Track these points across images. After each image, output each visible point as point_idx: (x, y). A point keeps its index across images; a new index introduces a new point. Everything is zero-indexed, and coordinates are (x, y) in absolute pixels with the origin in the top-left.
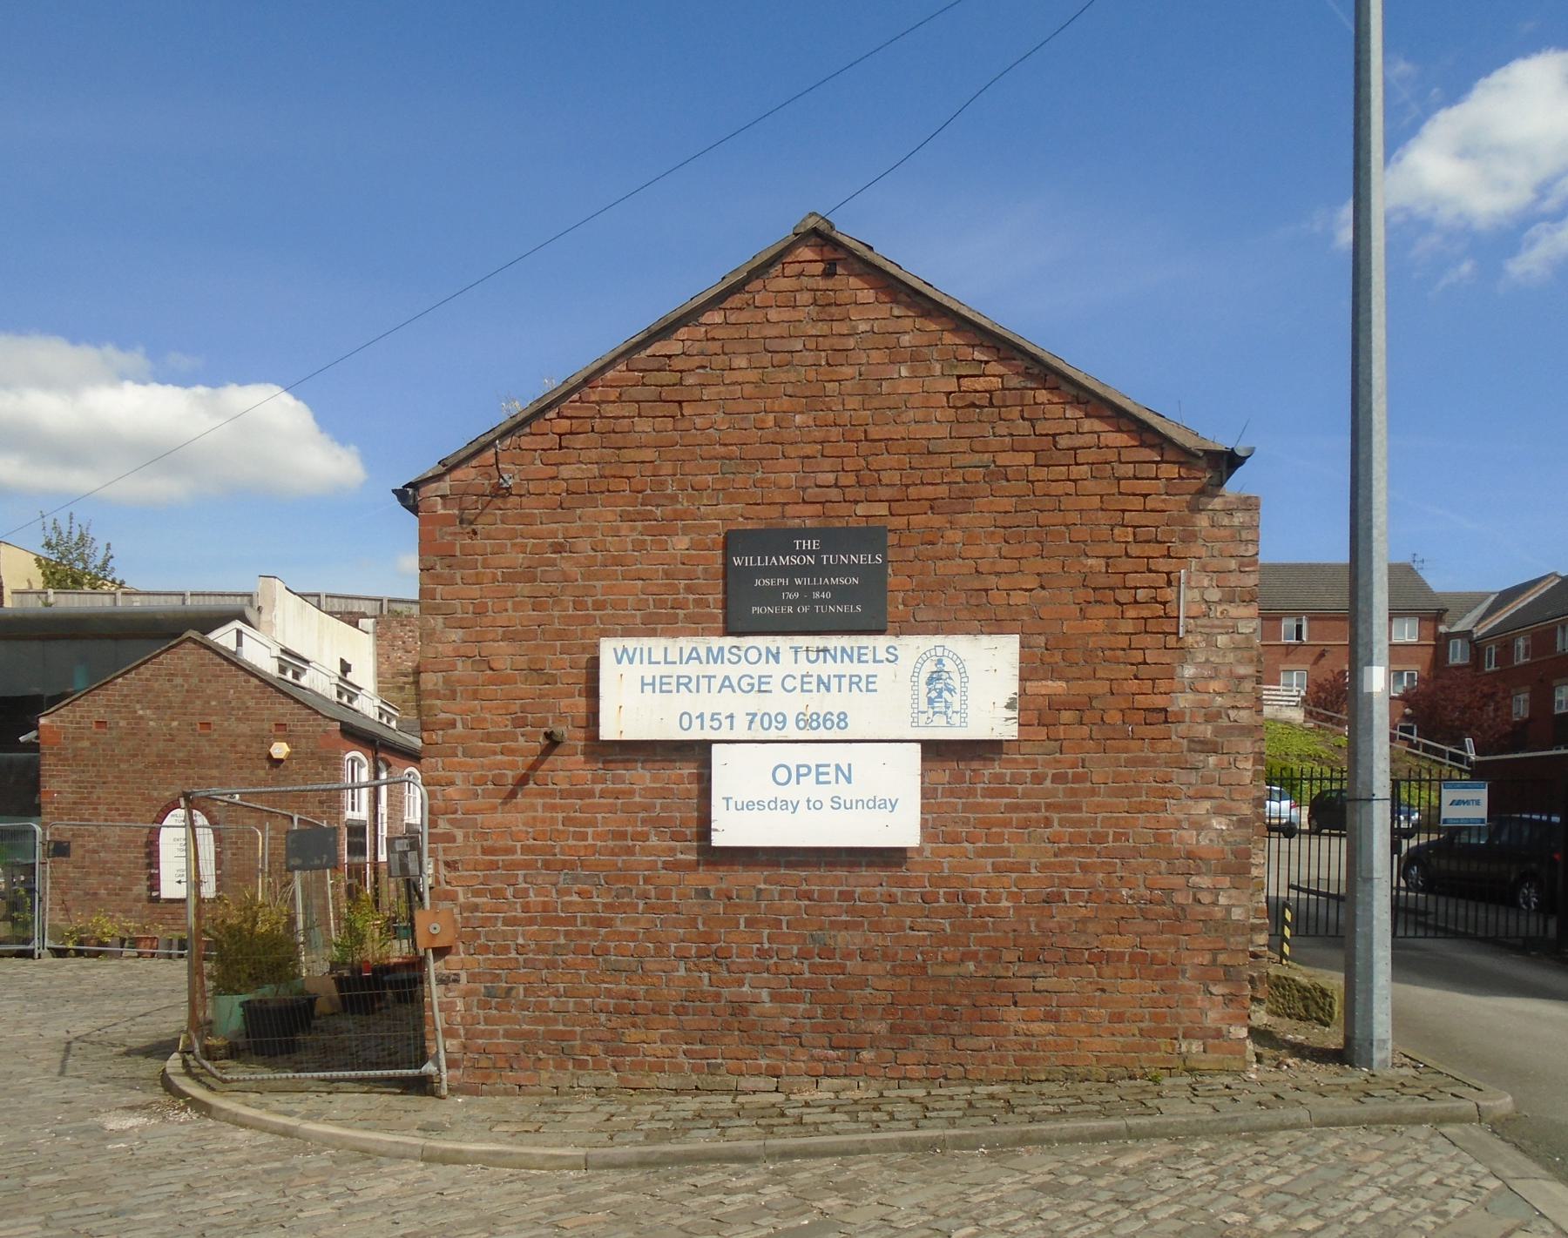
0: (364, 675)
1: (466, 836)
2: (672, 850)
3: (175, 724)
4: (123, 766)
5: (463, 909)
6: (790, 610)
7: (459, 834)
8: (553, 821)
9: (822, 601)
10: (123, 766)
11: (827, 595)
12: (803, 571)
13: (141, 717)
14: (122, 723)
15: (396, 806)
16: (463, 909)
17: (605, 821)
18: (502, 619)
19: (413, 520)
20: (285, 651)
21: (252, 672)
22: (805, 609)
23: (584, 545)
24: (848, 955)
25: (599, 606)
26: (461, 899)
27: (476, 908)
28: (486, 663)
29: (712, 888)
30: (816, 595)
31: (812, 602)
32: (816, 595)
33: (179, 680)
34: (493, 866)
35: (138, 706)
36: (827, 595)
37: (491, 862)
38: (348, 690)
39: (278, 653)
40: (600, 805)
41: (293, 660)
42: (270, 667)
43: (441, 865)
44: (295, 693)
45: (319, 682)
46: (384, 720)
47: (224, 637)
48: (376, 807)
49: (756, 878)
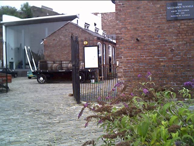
0: (99, 26)
1: (124, 57)
2: (159, 59)
3: (67, 39)
4: (58, 47)
5: (123, 70)
6: (177, 16)
7: (123, 57)
8: (138, 54)
9: (183, 14)
10: (58, 47)
11: (184, 13)
12: (180, 9)
13: (61, 38)
14: (58, 39)
15: (107, 53)
16: (123, 70)
17: (147, 54)
18: (129, 21)
19: (114, 5)
20: (85, 23)
21: (81, 28)
22: (180, 16)
23: (142, 7)
24: (190, 76)
25: (145, 17)
26: (123, 68)
27: (126, 69)
28: (126, 28)
29: (165, 65)
30: (182, 13)
31: (181, 14)
32: (182, 13)
33: (67, 31)
34: (128, 62)
35: (60, 36)
36: (184, 13)
37: (128, 62)
38: (97, 30)
39: (85, 24)
40: (146, 51)
41: (87, 25)
42: (83, 27)
43: (120, 63)
44: (88, 31)
45: (92, 28)
46: (104, 35)
47: (74, 21)
48: (103, 54)
49: (7, 38)
